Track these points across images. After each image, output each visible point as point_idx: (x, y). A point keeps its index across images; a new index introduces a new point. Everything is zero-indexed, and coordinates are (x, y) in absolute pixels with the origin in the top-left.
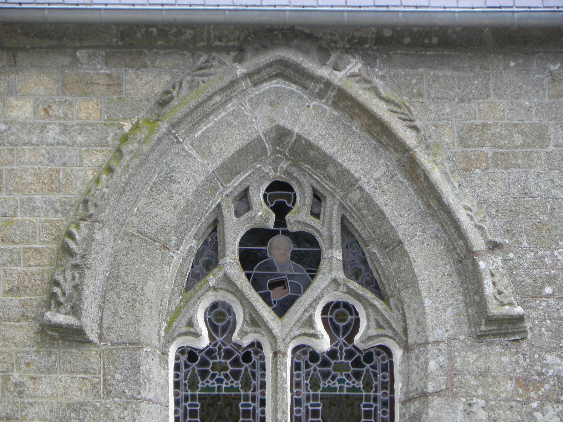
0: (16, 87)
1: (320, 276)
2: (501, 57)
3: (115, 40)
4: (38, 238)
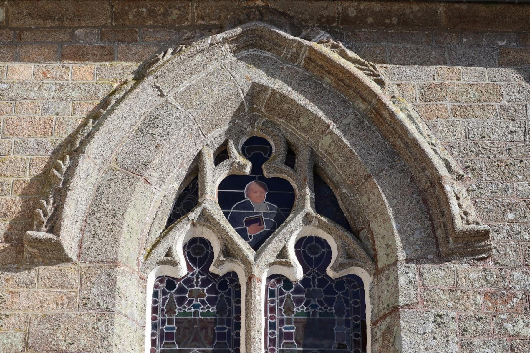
0: (20, 57)
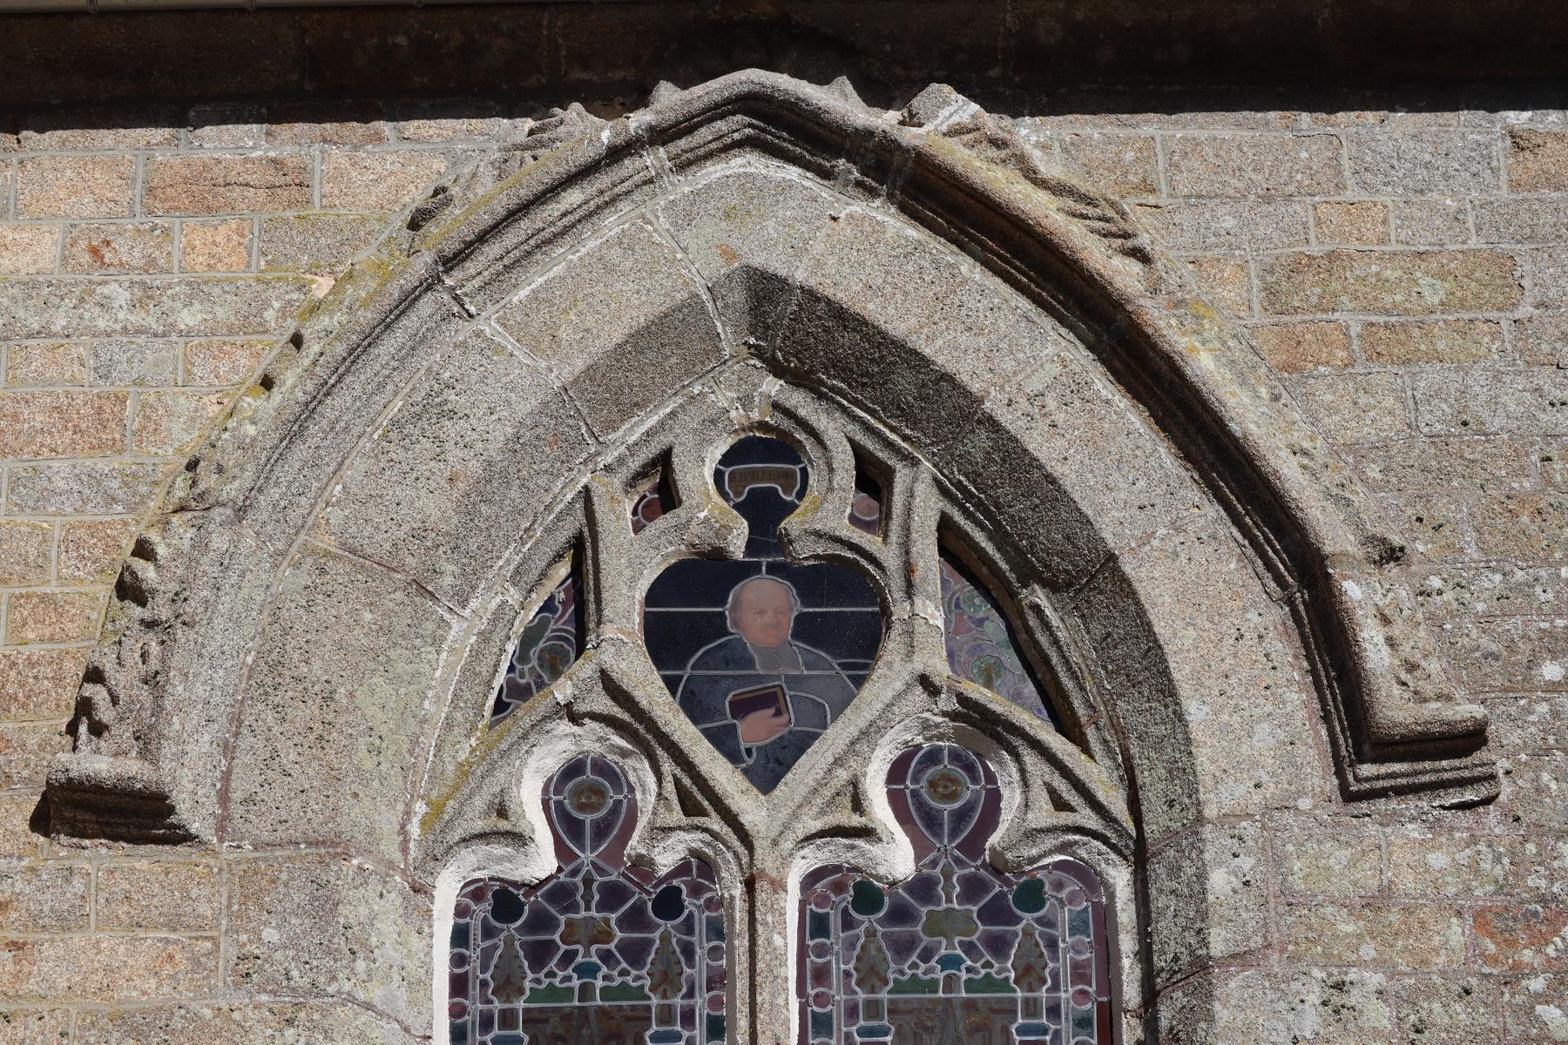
1: (880, 670)
2: (1368, 94)
3: (295, 77)
4: (53, 571)
